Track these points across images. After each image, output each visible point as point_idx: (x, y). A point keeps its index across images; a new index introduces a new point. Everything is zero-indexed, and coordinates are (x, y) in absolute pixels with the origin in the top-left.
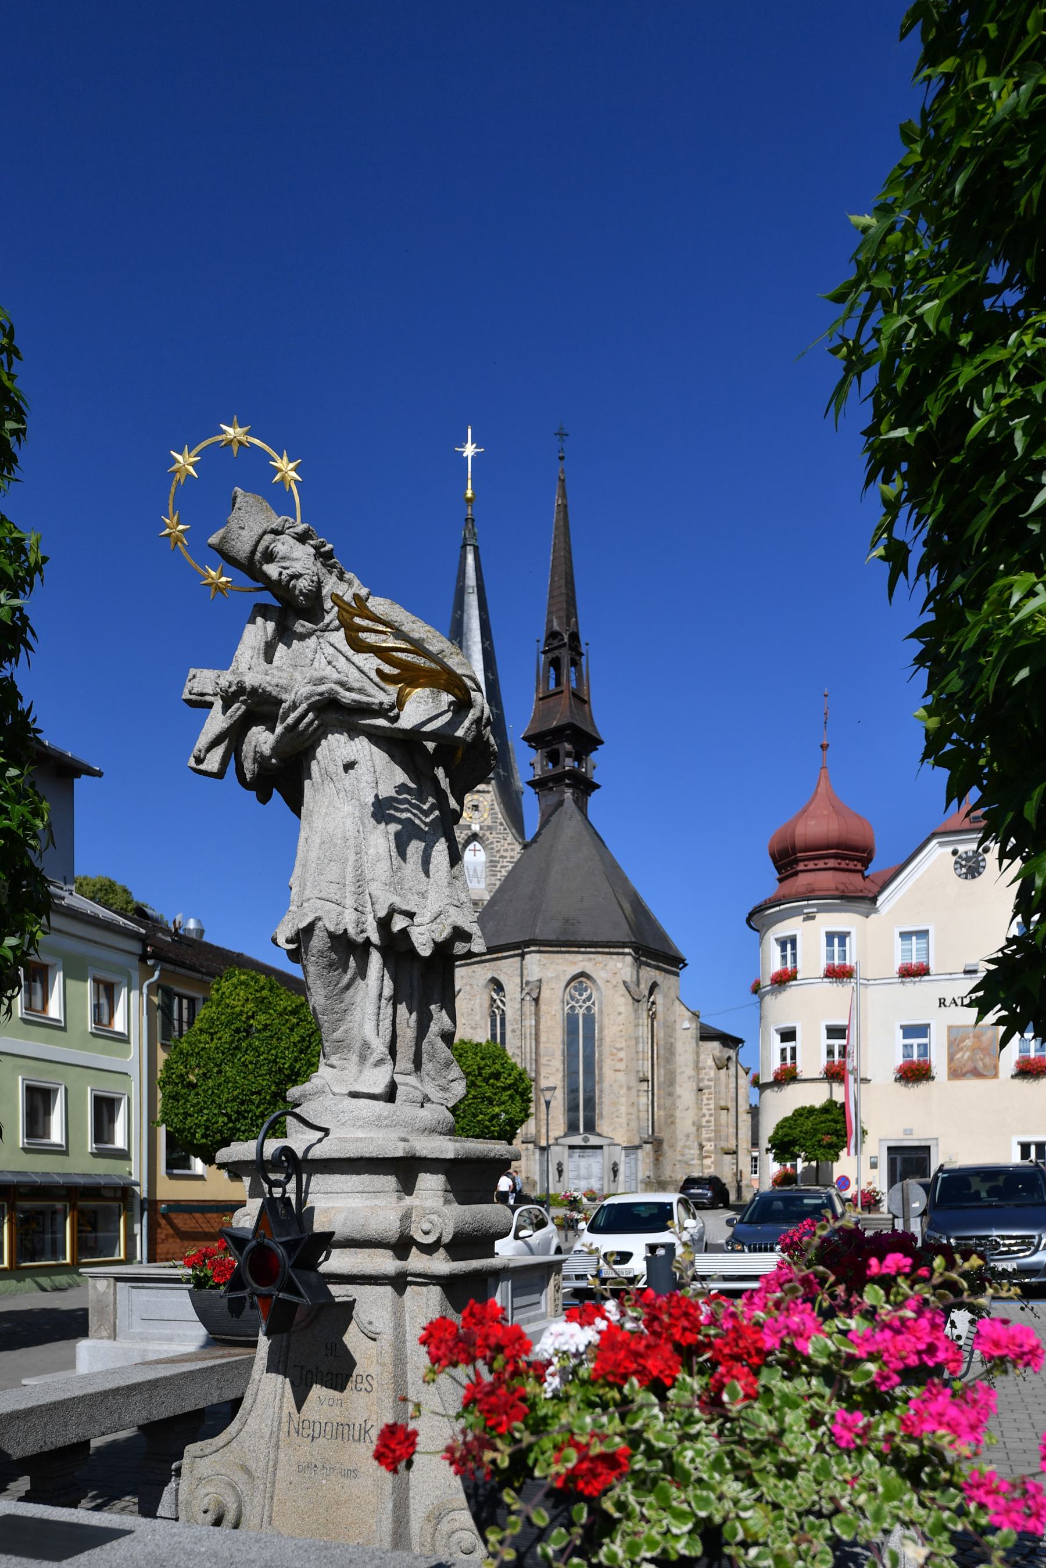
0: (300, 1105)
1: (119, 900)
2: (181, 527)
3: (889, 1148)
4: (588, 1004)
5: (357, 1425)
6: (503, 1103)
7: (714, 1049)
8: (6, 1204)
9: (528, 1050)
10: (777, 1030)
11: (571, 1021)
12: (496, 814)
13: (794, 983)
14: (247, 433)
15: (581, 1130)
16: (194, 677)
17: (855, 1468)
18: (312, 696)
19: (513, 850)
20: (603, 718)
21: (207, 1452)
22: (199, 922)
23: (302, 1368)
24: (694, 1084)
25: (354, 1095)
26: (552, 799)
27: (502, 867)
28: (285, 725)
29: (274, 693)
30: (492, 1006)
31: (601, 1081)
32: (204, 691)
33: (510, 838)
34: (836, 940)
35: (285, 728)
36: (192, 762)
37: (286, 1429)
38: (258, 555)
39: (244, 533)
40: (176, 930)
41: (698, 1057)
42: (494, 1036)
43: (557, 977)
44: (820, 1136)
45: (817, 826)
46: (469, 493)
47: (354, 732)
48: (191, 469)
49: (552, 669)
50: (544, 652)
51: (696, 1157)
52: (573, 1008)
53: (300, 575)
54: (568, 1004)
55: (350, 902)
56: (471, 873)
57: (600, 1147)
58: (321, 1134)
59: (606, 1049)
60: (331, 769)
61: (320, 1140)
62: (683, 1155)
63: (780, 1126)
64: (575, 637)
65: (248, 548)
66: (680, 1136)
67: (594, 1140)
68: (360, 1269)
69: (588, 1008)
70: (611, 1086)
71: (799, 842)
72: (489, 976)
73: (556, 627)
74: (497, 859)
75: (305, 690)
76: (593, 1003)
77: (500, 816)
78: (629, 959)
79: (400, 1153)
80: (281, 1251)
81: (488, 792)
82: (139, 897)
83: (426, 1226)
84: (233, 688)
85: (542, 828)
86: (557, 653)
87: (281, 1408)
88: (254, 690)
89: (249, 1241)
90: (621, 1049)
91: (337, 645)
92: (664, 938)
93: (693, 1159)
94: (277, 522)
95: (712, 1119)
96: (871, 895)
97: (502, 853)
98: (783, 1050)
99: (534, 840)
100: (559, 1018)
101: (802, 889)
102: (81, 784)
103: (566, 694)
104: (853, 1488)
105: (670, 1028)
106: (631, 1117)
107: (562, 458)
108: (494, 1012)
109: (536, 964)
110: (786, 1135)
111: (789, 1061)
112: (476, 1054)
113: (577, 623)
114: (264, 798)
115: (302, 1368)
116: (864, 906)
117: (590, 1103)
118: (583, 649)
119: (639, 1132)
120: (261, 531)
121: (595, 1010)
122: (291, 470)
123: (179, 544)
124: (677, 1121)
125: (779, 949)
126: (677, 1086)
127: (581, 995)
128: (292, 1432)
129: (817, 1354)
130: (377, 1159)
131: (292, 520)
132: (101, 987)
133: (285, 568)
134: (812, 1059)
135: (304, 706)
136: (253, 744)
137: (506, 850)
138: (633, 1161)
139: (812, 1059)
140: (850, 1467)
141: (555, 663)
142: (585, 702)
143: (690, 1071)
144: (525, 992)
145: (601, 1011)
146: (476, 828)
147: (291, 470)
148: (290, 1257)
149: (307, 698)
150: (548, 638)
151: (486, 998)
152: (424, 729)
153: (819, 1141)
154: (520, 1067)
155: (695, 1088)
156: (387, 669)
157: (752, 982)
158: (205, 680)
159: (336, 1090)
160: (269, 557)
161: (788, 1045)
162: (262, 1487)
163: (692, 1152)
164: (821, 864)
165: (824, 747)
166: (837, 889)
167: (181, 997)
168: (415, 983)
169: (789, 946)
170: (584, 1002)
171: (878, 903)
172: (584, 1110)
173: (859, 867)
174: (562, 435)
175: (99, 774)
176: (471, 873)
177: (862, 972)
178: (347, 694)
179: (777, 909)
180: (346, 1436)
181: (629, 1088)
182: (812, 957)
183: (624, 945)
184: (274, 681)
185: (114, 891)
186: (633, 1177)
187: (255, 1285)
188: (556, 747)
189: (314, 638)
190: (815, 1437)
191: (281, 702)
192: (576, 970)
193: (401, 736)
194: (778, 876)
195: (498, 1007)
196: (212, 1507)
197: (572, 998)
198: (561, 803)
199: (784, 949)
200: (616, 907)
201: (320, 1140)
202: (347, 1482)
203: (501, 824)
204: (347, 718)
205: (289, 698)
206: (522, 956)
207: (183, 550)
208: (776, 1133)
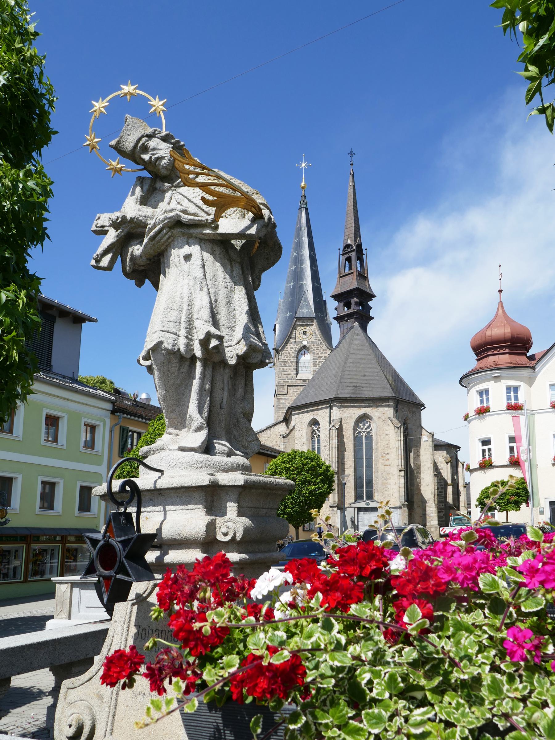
0: (147, 457)
1: (108, 387)
2: (96, 140)
3: (550, 502)
8: (25, 545)
9: (334, 456)
10: (479, 440)
12: (316, 335)
13: (487, 414)
14: (103, 100)
16: (99, 218)
17: (525, 688)
19: (326, 353)
21: (76, 685)
22: (148, 394)
25: (182, 449)
26: (346, 325)
27: (319, 362)
28: (148, 237)
29: (143, 221)
30: (312, 433)
32: (104, 224)
35: (149, 239)
36: (93, 262)
39: (130, 137)
40: (135, 399)
42: (314, 449)
43: (350, 417)
44: (508, 497)
47: (189, 240)
48: (103, 110)
49: (347, 262)
50: (342, 255)
51: (434, 512)
55: (183, 333)
56: (302, 365)
58: (160, 474)
61: (160, 477)
64: (359, 249)
67: (372, 504)
68: (178, 559)
69: (369, 432)
73: (349, 242)
75: (161, 217)
76: (371, 430)
77: (318, 336)
79: (207, 483)
80: (118, 547)
82: (118, 386)
83: (224, 530)
86: (350, 254)
89: (100, 541)
91: (183, 193)
92: (412, 394)
94: (150, 131)
95: (443, 490)
96: (531, 365)
97: (320, 355)
98: (484, 451)
99: (337, 347)
101: (492, 364)
102: (86, 326)
103: (355, 273)
104: (525, 706)
107: (352, 165)
108: (313, 436)
112: (301, 457)
113: (360, 240)
114: (140, 283)
116: (526, 373)
117: (370, 483)
120: (139, 136)
121: (373, 433)
122: (161, 105)
125: (479, 396)
127: (364, 425)
129: (488, 588)
130: (192, 487)
131: (159, 130)
132: (89, 428)
134: (500, 455)
137: (322, 353)
139: (500, 455)
140: (520, 686)
141: (349, 259)
144: (331, 425)
146: (305, 343)
147: (161, 105)
148: (124, 550)
149: (162, 221)
153: (508, 500)
154: (327, 463)
156: (210, 198)
157: (465, 414)
158: (105, 219)
159: (171, 448)
160: (145, 149)
163: (431, 509)
164: (502, 351)
167: (133, 432)
168: (226, 382)
169: (484, 396)
170: (366, 429)
171: (536, 370)
172: (366, 488)
175: (96, 321)
176: (302, 365)
177: (525, 408)
178: (186, 216)
184: (144, 214)
185: (106, 383)
187: (101, 570)
190: (487, 658)
193: (219, 238)
194: (476, 358)
196: (74, 723)
198: (352, 327)
201: (160, 477)
203: (319, 340)
204: (186, 230)
205: (151, 222)
206: (331, 408)
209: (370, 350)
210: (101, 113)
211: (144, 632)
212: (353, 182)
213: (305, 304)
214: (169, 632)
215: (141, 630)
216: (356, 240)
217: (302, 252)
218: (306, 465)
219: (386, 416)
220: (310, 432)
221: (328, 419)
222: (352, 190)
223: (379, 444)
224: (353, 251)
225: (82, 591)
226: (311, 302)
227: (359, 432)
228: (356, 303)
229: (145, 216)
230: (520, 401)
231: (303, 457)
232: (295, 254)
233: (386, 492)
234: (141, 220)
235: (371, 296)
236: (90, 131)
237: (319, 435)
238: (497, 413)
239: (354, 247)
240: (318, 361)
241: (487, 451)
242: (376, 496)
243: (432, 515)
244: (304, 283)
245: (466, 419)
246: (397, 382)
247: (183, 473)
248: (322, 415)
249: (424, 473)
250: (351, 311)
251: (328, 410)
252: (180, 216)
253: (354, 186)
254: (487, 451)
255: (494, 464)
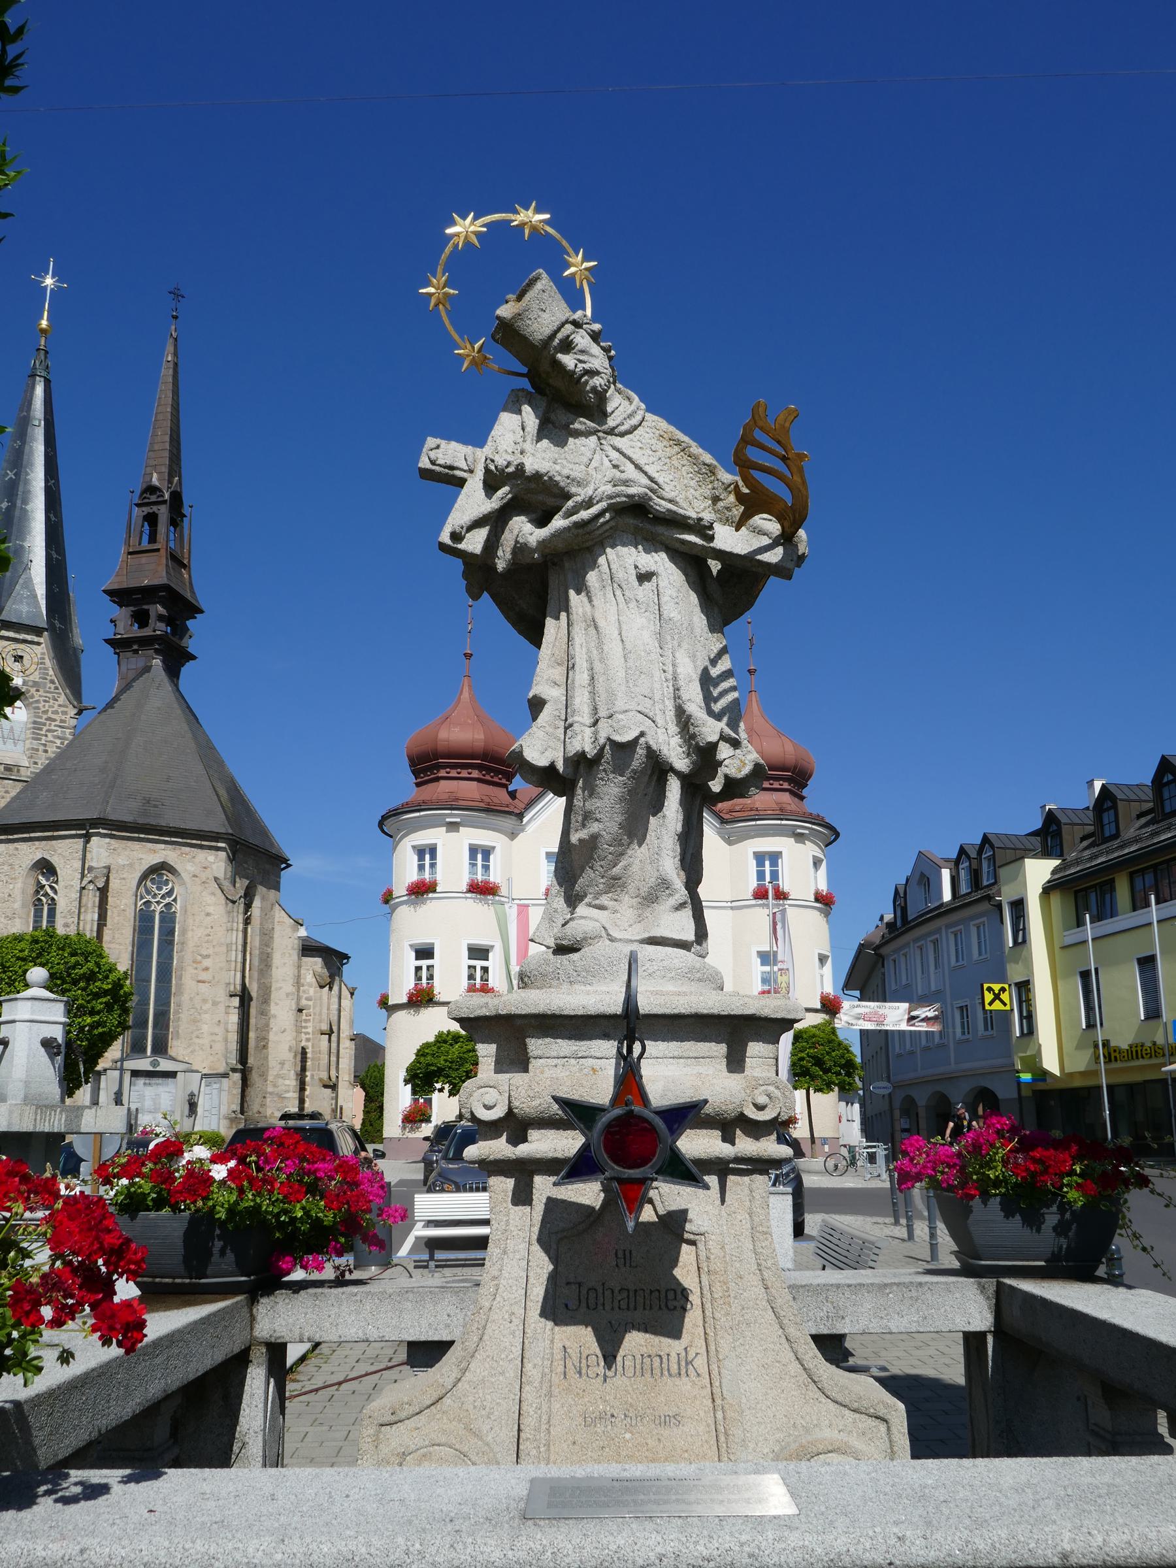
4: (168, 900)
5: (673, 1355)
6: (98, 1013)
7: (316, 963)
10: (411, 946)
11: (144, 921)
12: (46, 669)
13: (430, 895)
14: (475, 218)
15: (149, 1053)
18: (618, 495)
19: (65, 713)
20: (202, 584)
21: (403, 1415)
23: (580, 1284)
24: (293, 1002)
26: (135, 662)
27: (48, 731)
29: (562, 484)
30: (37, 892)
31: (180, 992)
32: (456, 464)
33: (62, 699)
34: (479, 856)
37: (561, 1369)
38: (556, 342)
39: (544, 315)
41: (299, 972)
43: (131, 865)
45: (461, 732)
46: (44, 323)
47: (652, 543)
52: (148, 903)
53: (597, 373)
54: (142, 898)
57: (172, 1075)
59: (188, 957)
60: (620, 575)
62: (275, 1086)
63: (421, 1053)
64: (177, 499)
65: (547, 331)
66: (272, 1062)
67: (165, 1065)
69: (168, 905)
70: (191, 999)
71: (441, 747)
72: (38, 856)
73: (155, 480)
74: (43, 721)
75: (609, 489)
76: (175, 900)
77: (51, 672)
78: (223, 854)
81: (39, 644)
84: (511, 469)
85: (122, 691)
86: (155, 509)
87: (552, 1342)
88: (537, 476)
90: (208, 956)
92: (264, 833)
93: (288, 1091)
97: (50, 714)
98: (418, 969)
100: (130, 914)
101: (445, 796)
103: (163, 552)
105: (267, 936)
106: (214, 1037)
108: (39, 900)
109: (101, 849)
110: (428, 1065)
111: (424, 981)
113: (180, 481)
115: (580, 1284)
116: (509, 822)
118: (186, 510)
119: (226, 1058)
120: (564, 319)
121: (178, 907)
123: (441, 306)
124: (270, 1044)
125: (416, 857)
126: (272, 1004)
127: (159, 889)
128: (571, 1372)
133: (581, 361)
135: (604, 504)
136: (515, 532)
137: (56, 712)
138: (215, 1092)
141: (151, 519)
142: (184, 566)
143: (289, 987)
145: (185, 910)
149: (610, 497)
150: (145, 491)
151: (32, 881)
152: (759, 557)
155: (294, 1007)
160: (567, 346)
161: (424, 963)
162: (534, 1452)
163: (287, 1082)
164: (464, 774)
165: (468, 656)
166: (482, 801)
169: (427, 857)
170: (163, 897)
171: (525, 820)
173: (504, 781)
174: (177, 294)
177: (504, 891)
179: (417, 814)
180: (657, 1371)
181: (215, 1004)
182: (453, 870)
183: (216, 837)
184: (565, 472)
186: (214, 1111)
188: (146, 607)
189: (593, 439)
191: (568, 496)
192: (155, 859)
195: (46, 895)
197: (148, 892)
198: (147, 669)
199: (421, 857)
200: (211, 792)
202: (666, 1432)
203: (52, 682)
206: (87, 838)
207: (443, 314)
208: (417, 1061)
209: (185, 727)
210: (468, 243)
211: (592, 1295)
212: (175, 354)
213: (26, 593)
214: (651, 1292)
215: (584, 1292)
216: (170, 482)
217: (27, 474)
218: (74, 967)
219: (209, 874)
220: (31, 889)
221: (78, 864)
222: (171, 372)
223: (190, 934)
224: (164, 502)
225: (557, 1329)
226: (41, 590)
227: (148, 903)
228: (160, 618)
229: (568, 477)
230: (495, 877)
231: (68, 950)
232: (11, 475)
233: (197, 1041)
234: (557, 483)
235: (194, 610)
236: (440, 269)
237: (53, 899)
238: (449, 895)
239: (167, 496)
240: (45, 728)
241: (424, 969)
242: (176, 1047)
243: (287, 1095)
244: (26, 544)
245: (386, 902)
246: (237, 805)
247: (670, 987)
248: (64, 853)
249: (277, 1004)
250: (147, 632)
251: (80, 842)
252: (650, 499)
253: (176, 364)
254: (424, 969)
255: (438, 998)
